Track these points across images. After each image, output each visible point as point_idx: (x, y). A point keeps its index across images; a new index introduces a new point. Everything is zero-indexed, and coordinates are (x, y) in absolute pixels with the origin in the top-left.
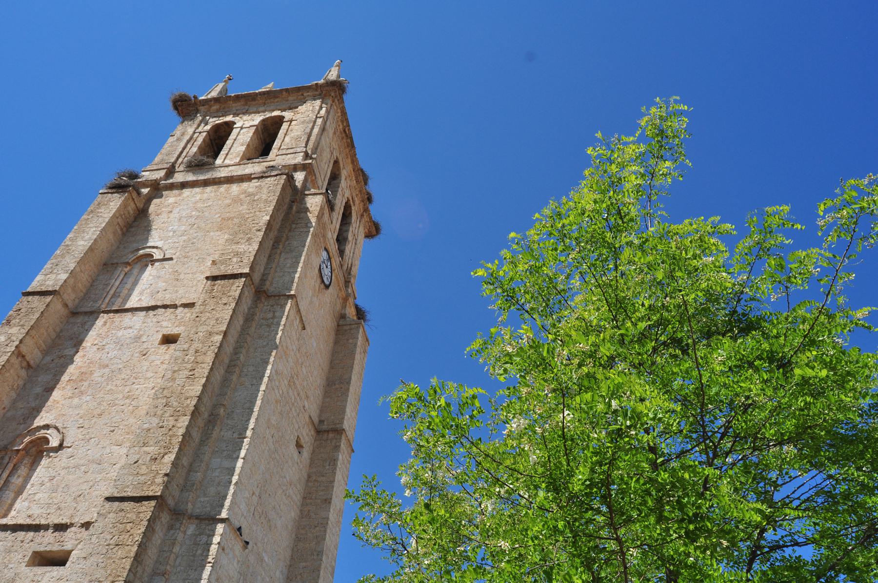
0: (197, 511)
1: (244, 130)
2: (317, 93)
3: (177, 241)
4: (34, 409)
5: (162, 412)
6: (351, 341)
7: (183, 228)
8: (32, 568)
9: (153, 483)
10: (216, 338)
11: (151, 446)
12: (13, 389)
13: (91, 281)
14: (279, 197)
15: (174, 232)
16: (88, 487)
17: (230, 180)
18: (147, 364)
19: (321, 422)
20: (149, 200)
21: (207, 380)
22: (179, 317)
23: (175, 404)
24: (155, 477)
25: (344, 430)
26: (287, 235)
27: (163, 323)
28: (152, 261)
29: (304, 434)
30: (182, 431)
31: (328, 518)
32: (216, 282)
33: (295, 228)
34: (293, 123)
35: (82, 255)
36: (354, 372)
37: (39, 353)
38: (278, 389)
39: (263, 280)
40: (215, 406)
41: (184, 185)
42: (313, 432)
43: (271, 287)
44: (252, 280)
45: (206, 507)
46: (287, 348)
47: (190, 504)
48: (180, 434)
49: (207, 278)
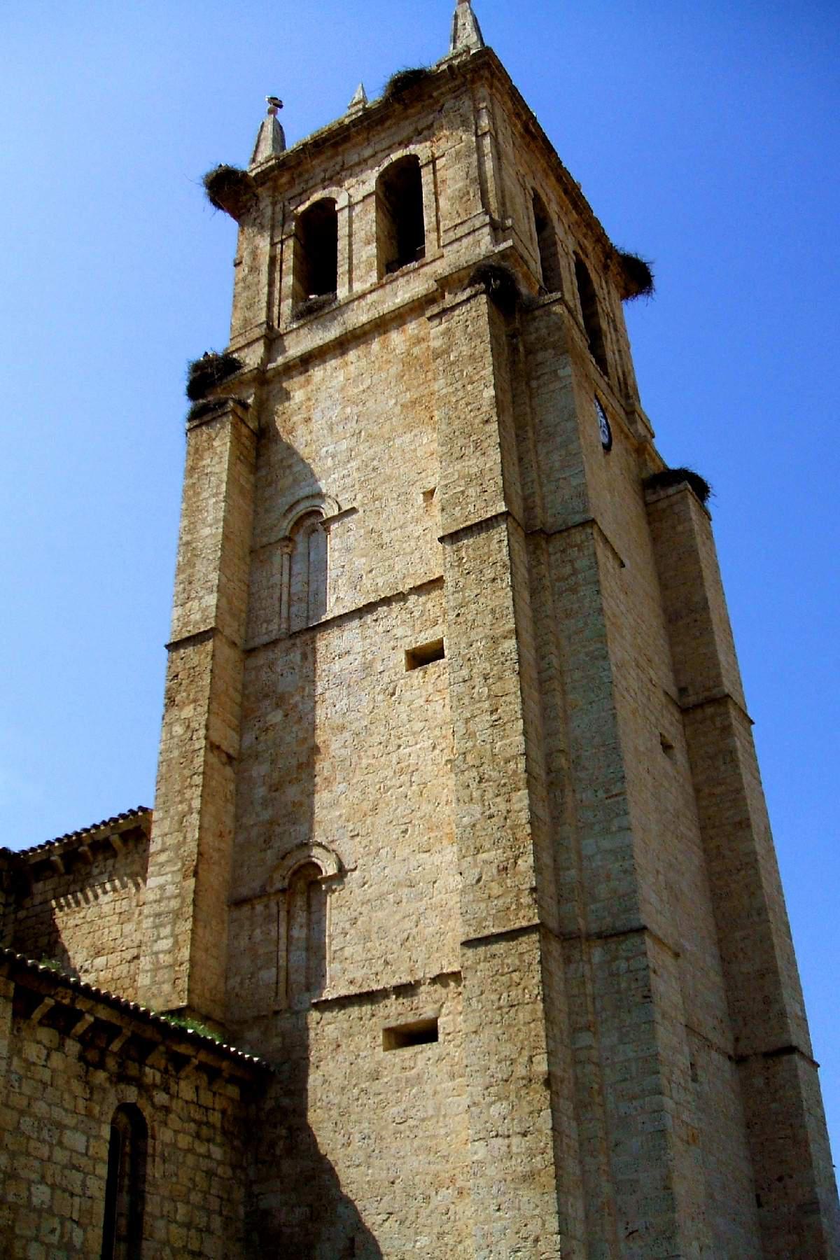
0: (594, 928)
1: (358, 209)
2: (457, 82)
3: (345, 472)
4: (271, 823)
5: (479, 792)
6: (680, 528)
7: (344, 445)
8: (394, 1051)
9: (519, 905)
10: (506, 646)
11: (489, 850)
12: (227, 801)
13: (244, 588)
14: (491, 342)
15: (333, 457)
16: (413, 924)
17: (382, 325)
18: (403, 708)
19: (682, 691)
20: (264, 406)
21: (525, 723)
22: (416, 614)
23: (494, 774)
24: (518, 896)
25: (728, 696)
26: (531, 407)
27: (395, 631)
28: (323, 523)
29: (667, 725)
30: (524, 816)
31: (755, 853)
32: (460, 544)
33: (538, 388)
34: (439, 163)
35: (219, 554)
36: (707, 584)
37: (234, 734)
38: (628, 691)
39: (528, 509)
40: (549, 756)
41: (307, 361)
42: (677, 715)
43: (548, 517)
44: (514, 518)
45: (604, 918)
46: (615, 616)
47: (580, 920)
48: (524, 821)
49: (441, 540)
